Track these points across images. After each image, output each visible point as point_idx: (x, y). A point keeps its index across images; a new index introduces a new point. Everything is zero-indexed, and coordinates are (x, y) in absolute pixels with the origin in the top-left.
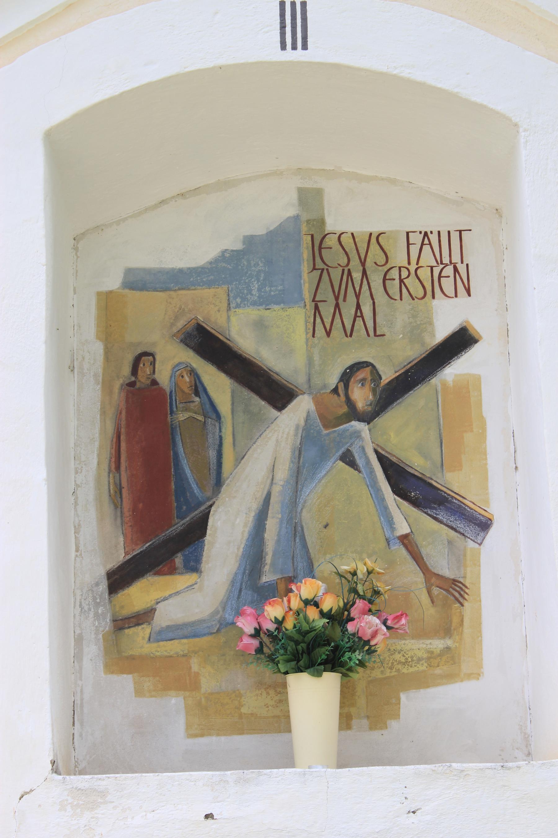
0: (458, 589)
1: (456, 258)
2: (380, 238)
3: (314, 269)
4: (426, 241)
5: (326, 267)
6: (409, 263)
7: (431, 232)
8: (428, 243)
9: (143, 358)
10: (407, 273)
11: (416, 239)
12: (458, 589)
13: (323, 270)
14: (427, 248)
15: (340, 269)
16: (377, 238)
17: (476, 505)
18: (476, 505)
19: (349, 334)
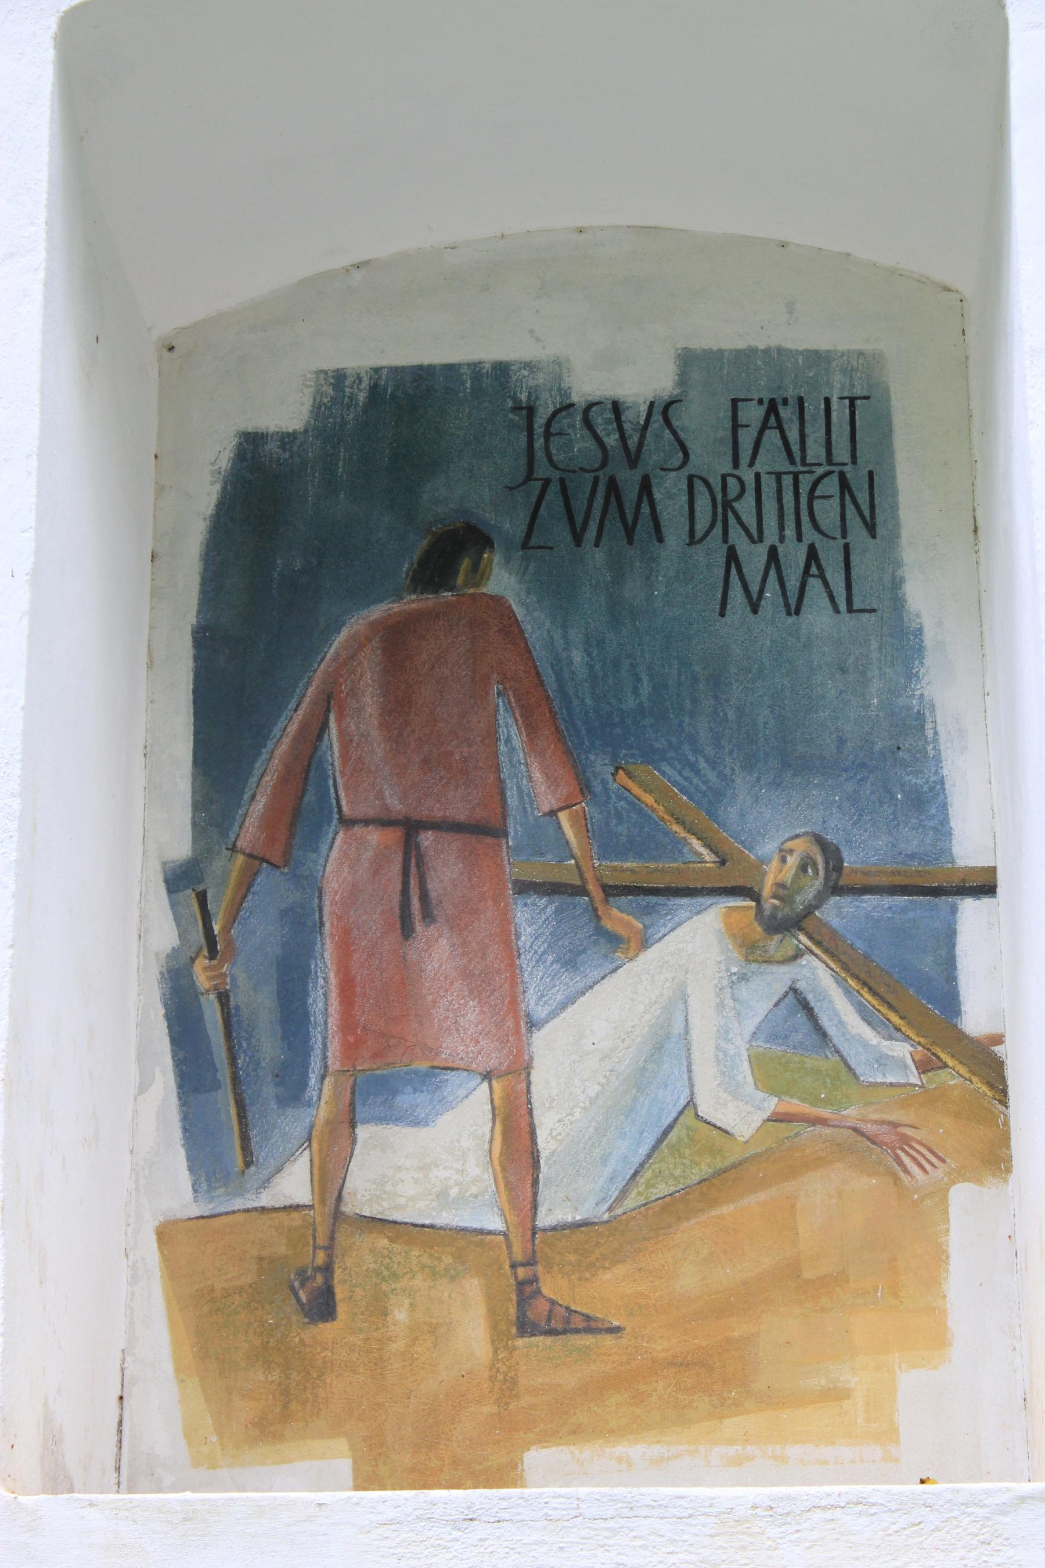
0: (914, 1153)
1: (842, 453)
2: (671, 411)
3: (529, 477)
4: (772, 420)
5: (556, 475)
6: (736, 464)
7: (785, 402)
8: (775, 425)
9: (591, 414)
10: (738, 489)
11: (753, 414)
12: (914, 1153)
13: (547, 482)
14: (772, 437)
15: (590, 477)
16: (665, 414)
17: (121, 1415)
18: (121, 1415)
19: (755, 536)
